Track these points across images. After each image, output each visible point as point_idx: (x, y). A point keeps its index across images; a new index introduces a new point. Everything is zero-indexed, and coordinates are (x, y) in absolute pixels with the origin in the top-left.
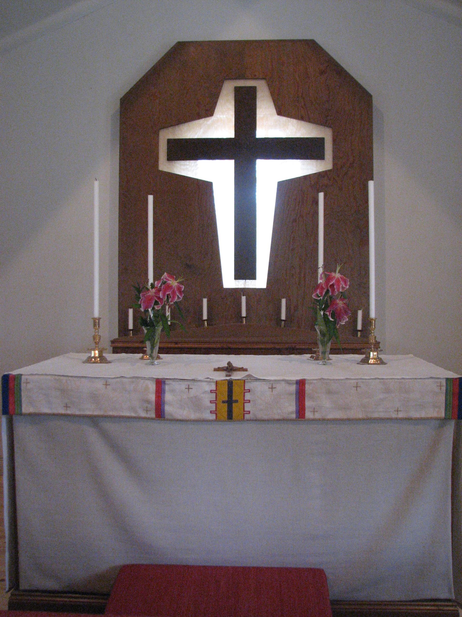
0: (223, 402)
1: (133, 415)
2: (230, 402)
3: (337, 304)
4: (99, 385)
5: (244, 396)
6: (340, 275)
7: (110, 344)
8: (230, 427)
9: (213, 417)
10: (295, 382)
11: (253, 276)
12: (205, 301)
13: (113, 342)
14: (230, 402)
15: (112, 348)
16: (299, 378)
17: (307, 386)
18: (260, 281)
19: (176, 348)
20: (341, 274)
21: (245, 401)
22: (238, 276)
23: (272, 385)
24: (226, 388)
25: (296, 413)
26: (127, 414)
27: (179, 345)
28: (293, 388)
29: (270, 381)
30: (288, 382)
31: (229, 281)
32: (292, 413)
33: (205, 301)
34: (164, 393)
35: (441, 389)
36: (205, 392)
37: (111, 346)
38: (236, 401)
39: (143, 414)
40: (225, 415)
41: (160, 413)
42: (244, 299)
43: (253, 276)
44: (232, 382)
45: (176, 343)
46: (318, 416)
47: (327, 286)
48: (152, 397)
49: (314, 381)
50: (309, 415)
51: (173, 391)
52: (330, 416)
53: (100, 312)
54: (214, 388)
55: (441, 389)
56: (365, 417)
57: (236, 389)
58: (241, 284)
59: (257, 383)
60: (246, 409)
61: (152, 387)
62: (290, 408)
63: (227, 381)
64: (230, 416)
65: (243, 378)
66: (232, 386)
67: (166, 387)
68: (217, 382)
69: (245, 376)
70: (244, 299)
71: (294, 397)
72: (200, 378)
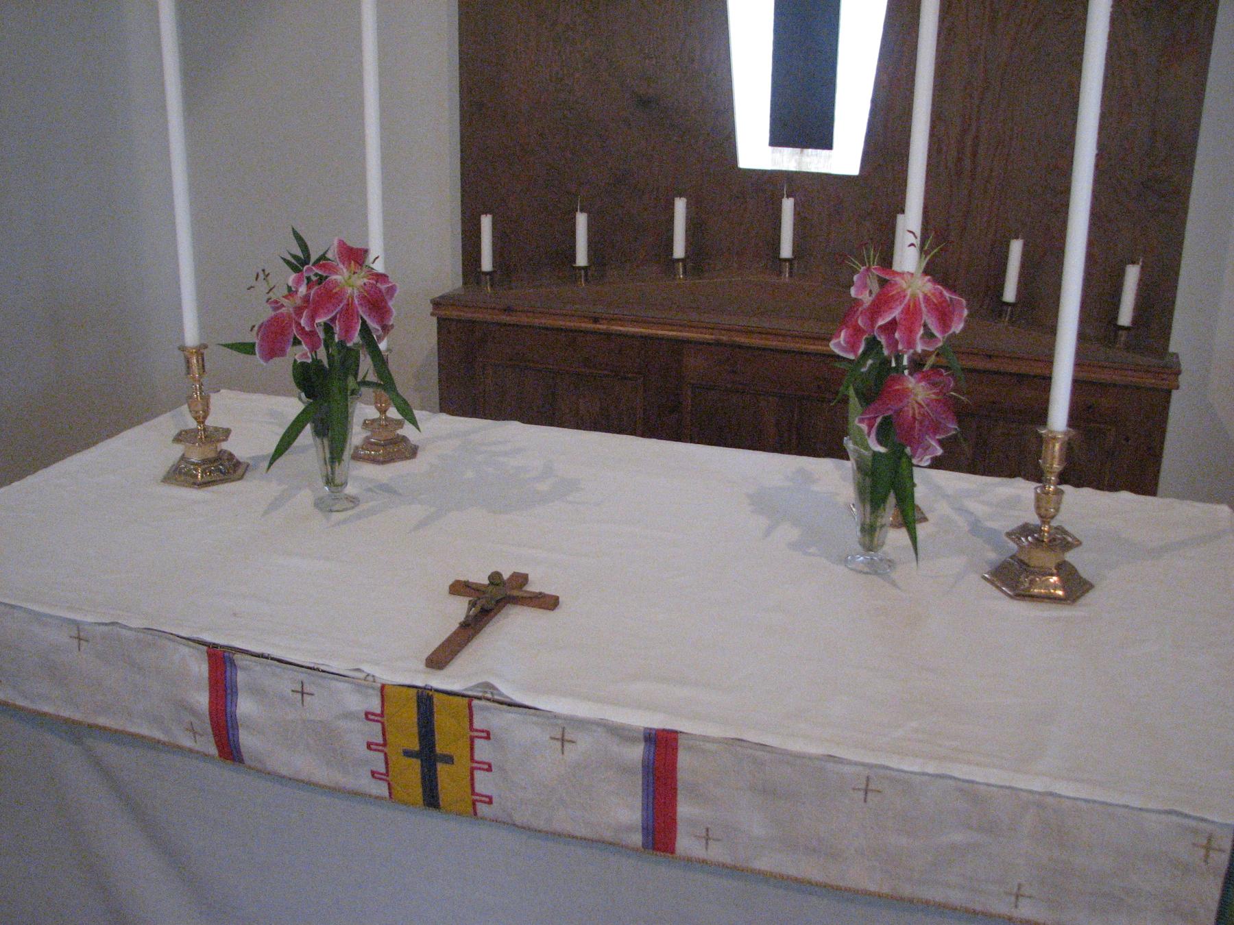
0: (408, 754)
1: (159, 735)
2: (428, 755)
3: (903, 394)
4: (62, 637)
5: (472, 749)
6: (930, 286)
7: (430, 308)
8: (431, 824)
9: (381, 789)
10: (641, 736)
11: (822, 139)
12: (680, 205)
13: (437, 304)
14: (428, 755)
15: (435, 320)
16: (658, 721)
17: (684, 760)
18: (844, 156)
19: (594, 332)
20: (936, 281)
21: (476, 766)
22: (781, 136)
23: (564, 731)
24: (411, 715)
25: (645, 829)
26: (145, 731)
27: (602, 327)
28: (636, 753)
29: (552, 717)
30: (619, 732)
31: (755, 150)
32: (629, 829)
33: (680, 205)
34: (235, 693)
35: (1207, 856)
36: (348, 715)
37: (432, 314)
38: (449, 760)
39: (187, 742)
40: (417, 792)
41: (229, 749)
42: (788, 205)
43: (822, 139)
44: (430, 698)
45: (596, 320)
46: (717, 853)
47: (872, 326)
48: (202, 700)
49: (708, 746)
50: (685, 843)
51: (258, 692)
52: (763, 864)
53: (203, 326)
54: (375, 705)
55: (1207, 856)
56: (886, 890)
57: (442, 721)
58: (788, 160)
59: (511, 716)
60: (479, 788)
61: (200, 668)
62: (626, 812)
63: (413, 692)
64: (431, 799)
65: (471, 689)
66: (432, 713)
67: (239, 673)
68: (383, 687)
69: (478, 686)
70: (788, 205)
71: (637, 782)
72: (335, 666)
